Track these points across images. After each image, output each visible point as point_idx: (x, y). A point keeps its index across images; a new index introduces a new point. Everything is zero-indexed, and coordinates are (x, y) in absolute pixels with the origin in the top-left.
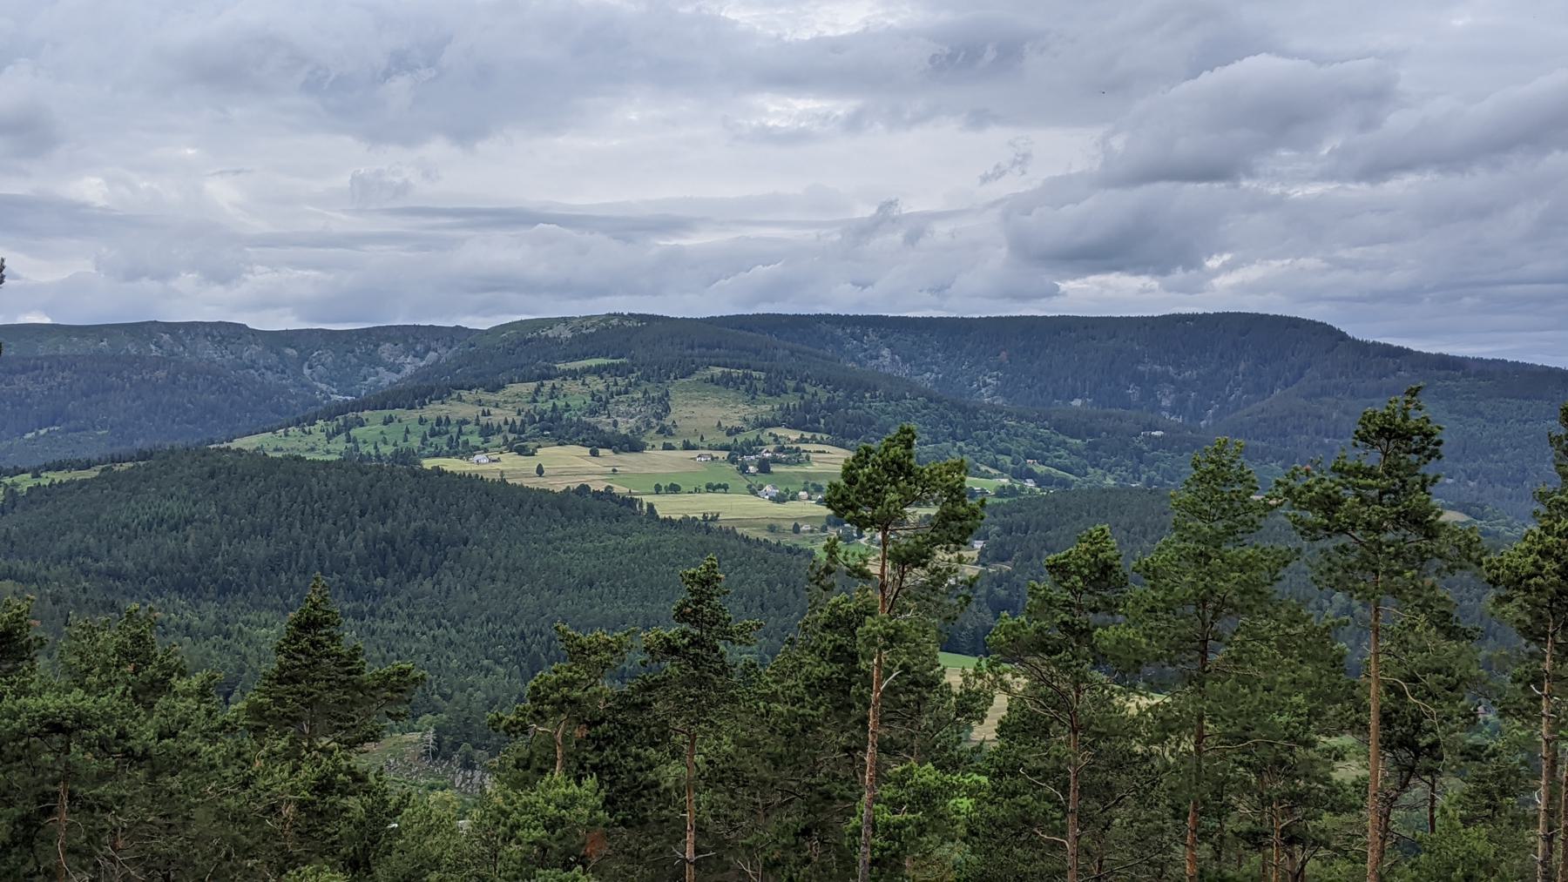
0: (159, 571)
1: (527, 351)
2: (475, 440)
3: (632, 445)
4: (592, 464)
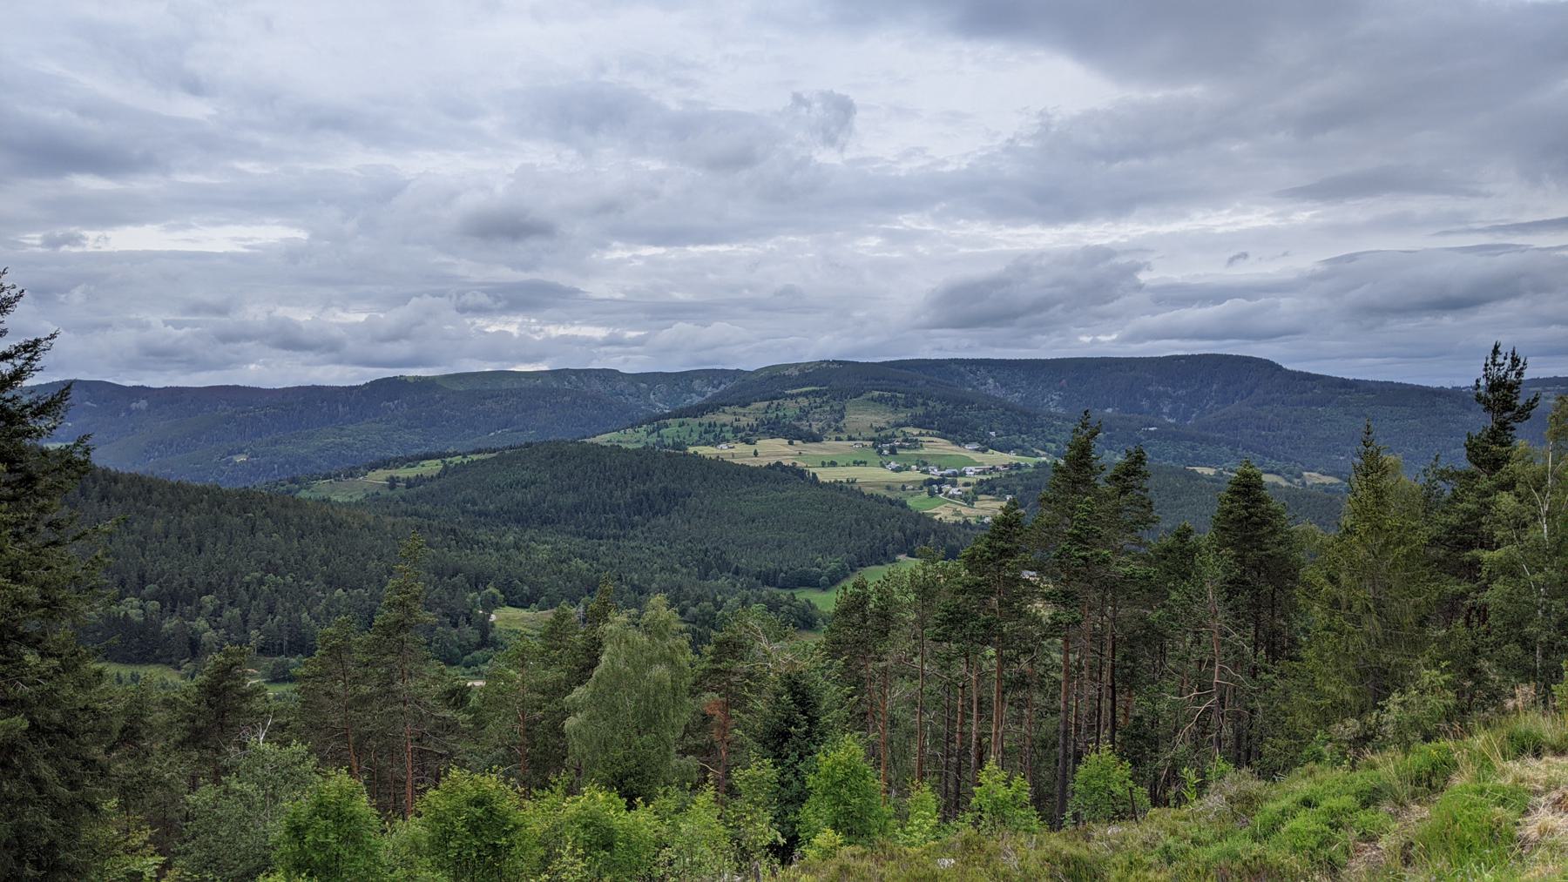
0: (509, 511)
1: (772, 384)
2: (729, 435)
3: (815, 439)
4: (789, 450)
